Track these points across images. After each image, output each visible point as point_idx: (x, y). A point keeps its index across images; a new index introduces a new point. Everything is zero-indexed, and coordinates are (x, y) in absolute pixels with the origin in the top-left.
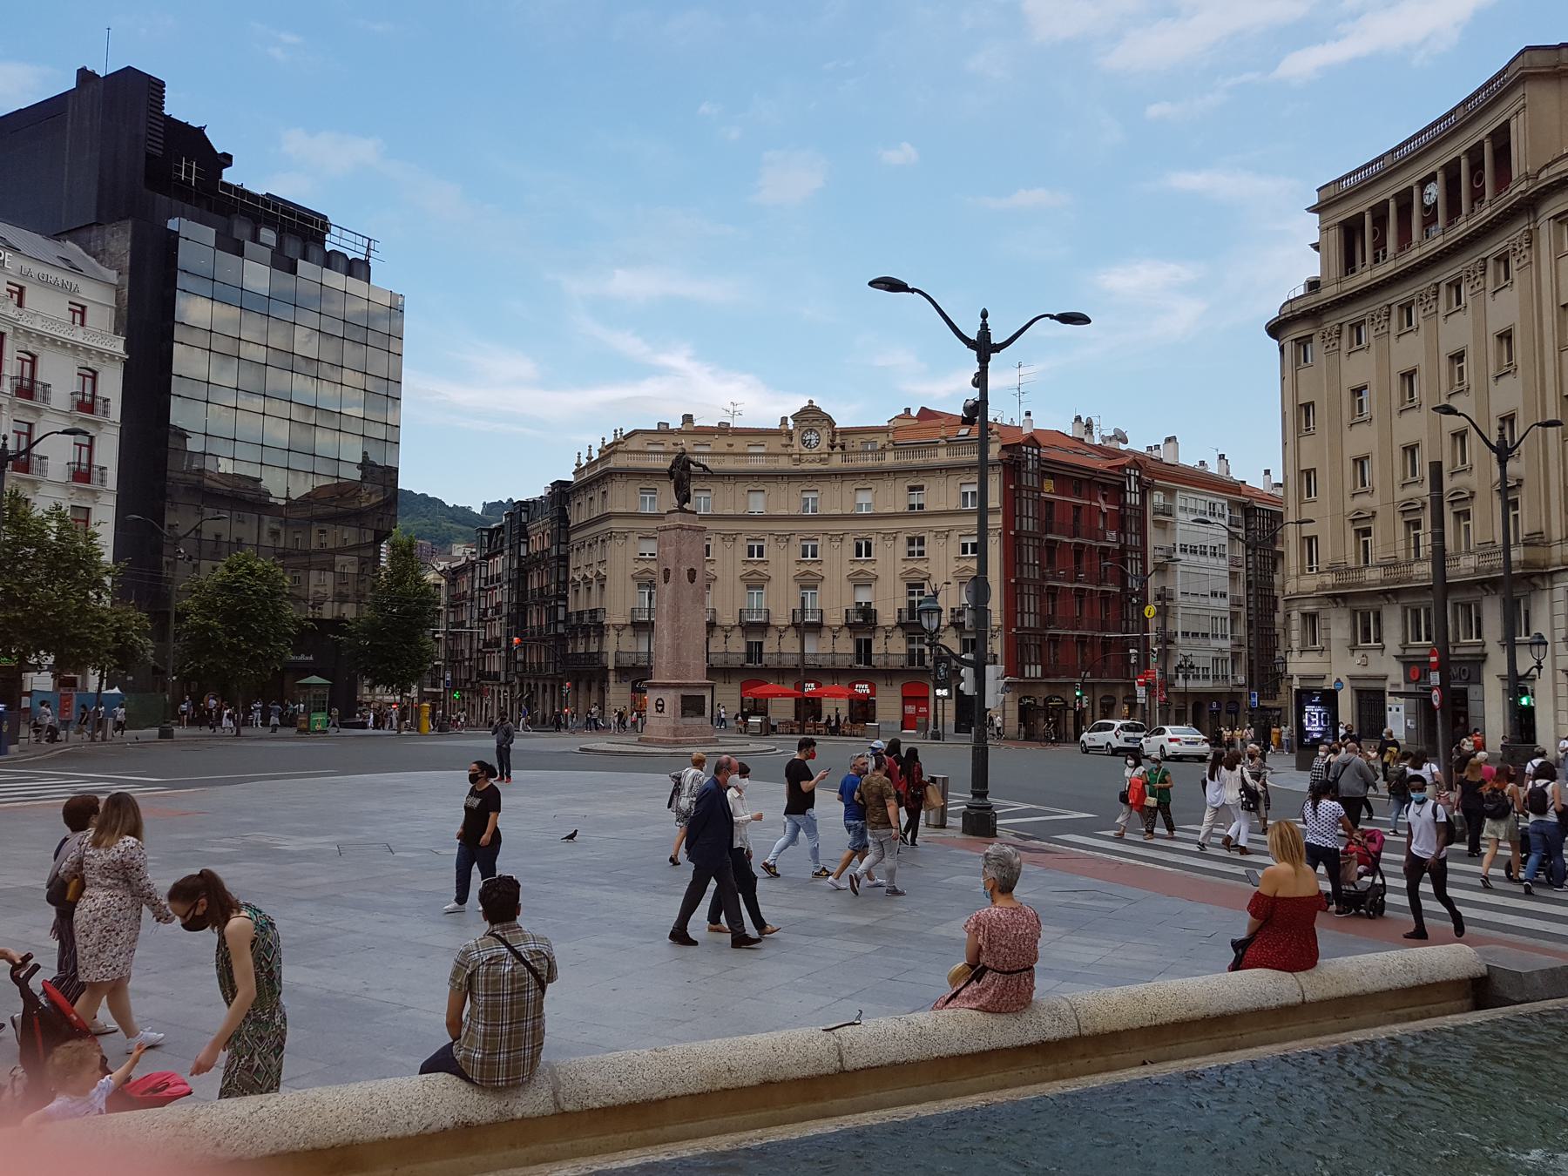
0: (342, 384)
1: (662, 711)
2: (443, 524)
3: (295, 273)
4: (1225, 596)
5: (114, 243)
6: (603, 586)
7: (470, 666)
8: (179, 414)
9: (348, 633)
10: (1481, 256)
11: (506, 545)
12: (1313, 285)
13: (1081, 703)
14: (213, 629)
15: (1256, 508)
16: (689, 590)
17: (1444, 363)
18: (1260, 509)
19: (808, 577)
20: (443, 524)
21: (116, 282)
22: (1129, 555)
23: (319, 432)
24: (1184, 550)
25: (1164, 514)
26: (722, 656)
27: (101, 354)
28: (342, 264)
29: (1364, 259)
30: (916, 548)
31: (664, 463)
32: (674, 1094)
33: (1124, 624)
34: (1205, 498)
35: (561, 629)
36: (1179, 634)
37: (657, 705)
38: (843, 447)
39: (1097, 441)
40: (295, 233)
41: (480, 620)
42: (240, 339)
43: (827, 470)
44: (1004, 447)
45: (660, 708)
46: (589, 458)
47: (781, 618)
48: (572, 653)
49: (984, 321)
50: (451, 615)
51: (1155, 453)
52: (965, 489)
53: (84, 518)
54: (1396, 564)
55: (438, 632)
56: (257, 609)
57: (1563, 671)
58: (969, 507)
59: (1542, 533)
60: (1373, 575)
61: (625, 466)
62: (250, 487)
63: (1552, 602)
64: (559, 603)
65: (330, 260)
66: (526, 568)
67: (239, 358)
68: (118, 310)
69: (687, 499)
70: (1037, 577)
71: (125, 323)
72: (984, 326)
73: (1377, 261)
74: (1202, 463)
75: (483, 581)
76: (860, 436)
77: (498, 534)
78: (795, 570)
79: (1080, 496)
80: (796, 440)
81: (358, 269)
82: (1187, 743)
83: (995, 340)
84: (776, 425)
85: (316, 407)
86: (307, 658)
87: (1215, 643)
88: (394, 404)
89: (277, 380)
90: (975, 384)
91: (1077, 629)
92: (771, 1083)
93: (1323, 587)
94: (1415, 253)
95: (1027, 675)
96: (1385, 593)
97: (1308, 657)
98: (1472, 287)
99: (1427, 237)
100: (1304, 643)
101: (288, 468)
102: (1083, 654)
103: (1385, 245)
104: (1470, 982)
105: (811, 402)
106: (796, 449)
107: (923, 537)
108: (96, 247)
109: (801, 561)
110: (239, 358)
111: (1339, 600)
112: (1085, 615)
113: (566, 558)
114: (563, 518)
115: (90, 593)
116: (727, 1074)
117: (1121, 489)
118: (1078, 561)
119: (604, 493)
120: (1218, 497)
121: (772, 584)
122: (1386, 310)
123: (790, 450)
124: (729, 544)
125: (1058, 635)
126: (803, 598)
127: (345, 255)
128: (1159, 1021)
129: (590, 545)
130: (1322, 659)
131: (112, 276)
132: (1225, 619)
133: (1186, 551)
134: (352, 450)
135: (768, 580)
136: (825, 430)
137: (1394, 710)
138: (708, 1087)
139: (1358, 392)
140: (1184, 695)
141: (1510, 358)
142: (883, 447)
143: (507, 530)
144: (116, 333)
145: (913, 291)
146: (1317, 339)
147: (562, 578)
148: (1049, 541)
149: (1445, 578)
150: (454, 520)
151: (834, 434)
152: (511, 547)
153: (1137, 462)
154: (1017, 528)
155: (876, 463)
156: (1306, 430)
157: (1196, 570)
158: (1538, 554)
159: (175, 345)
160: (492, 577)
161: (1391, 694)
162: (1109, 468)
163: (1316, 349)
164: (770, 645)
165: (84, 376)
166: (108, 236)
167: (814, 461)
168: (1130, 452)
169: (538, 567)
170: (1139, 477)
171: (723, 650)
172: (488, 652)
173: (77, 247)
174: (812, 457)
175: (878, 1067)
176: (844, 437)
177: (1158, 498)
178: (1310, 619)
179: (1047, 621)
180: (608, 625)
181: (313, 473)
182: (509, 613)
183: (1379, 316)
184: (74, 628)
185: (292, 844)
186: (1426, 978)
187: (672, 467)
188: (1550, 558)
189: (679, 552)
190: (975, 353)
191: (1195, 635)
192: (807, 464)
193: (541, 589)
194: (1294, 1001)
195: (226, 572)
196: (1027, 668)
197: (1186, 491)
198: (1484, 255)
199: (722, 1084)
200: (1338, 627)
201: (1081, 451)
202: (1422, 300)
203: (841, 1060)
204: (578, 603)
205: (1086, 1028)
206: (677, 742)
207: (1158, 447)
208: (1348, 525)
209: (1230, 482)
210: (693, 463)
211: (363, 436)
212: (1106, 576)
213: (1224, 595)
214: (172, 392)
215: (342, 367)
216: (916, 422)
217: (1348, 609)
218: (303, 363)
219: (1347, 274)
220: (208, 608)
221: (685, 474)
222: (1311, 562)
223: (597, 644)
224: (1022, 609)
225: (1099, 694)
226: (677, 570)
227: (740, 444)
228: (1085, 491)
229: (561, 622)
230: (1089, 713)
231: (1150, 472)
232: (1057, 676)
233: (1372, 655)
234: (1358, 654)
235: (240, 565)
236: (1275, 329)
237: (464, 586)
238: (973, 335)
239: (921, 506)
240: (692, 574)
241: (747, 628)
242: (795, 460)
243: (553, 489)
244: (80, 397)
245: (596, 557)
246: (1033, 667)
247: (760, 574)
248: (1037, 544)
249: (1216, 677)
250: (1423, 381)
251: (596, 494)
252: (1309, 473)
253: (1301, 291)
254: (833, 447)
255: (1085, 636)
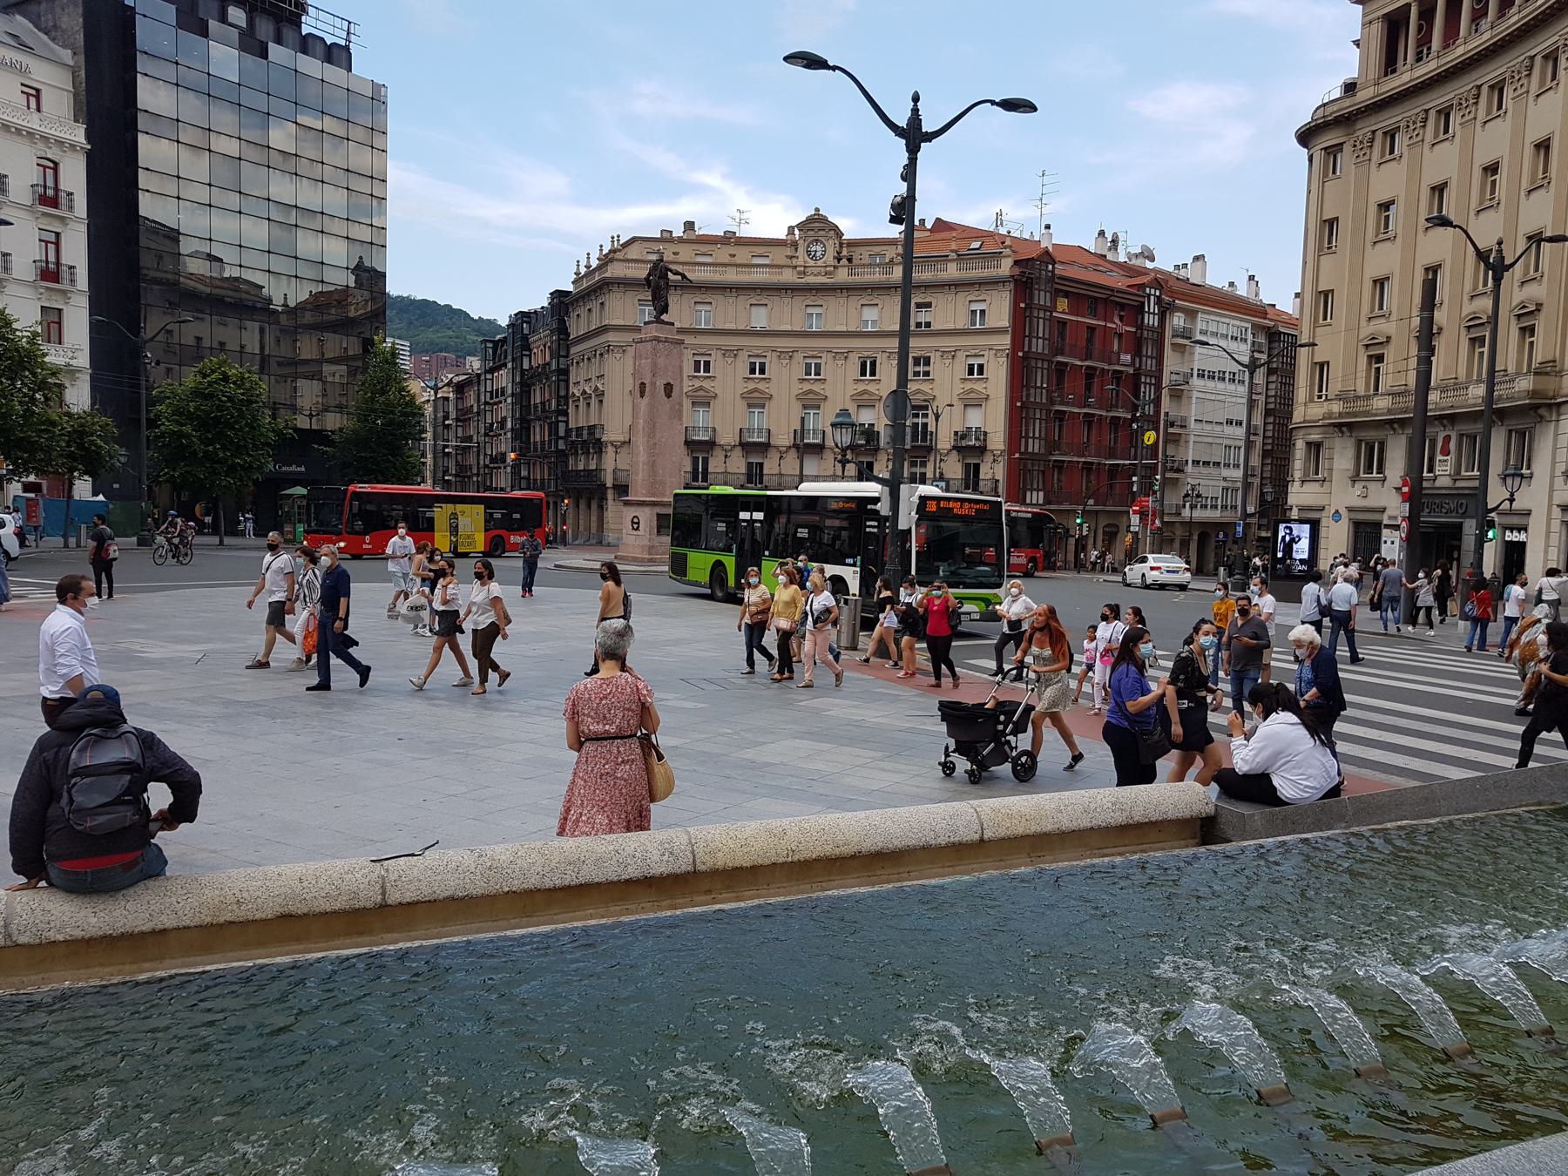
0: (323, 182)
1: (638, 529)
2: (468, 337)
3: (266, 57)
4: (1241, 424)
5: (65, 19)
6: (601, 401)
7: (478, 481)
8: (148, 207)
9: (331, 443)
10: (1528, 54)
11: (510, 357)
12: (1350, 88)
13: (1081, 530)
14: (187, 436)
15: (1281, 333)
16: (665, 404)
17: (1477, 173)
18: (1285, 334)
19: (811, 396)
20: (468, 337)
21: (71, 63)
22: (1143, 380)
23: (300, 231)
24: (1201, 375)
25: (1183, 337)
26: (776, 478)
27: (60, 143)
28: (319, 49)
29: (1405, 59)
30: (921, 369)
31: (642, 272)
32: (162, 927)
33: (1133, 450)
34: (1227, 320)
35: (561, 445)
36: (1190, 462)
37: (633, 522)
38: (850, 260)
39: (1122, 258)
40: (269, 13)
41: (486, 435)
42: (209, 130)
43: (833, 284)
44: (1016, 263)
45: (635, 526)
46: (588, 267)
47: (783, 439)
48: (584, 470)
49: (916, 105)
50: (460, 429)
51: (1183, 273)
52: (974, 307)
53: (57, 320)
54: (1406, 391)
55: (447, 446)
56: (232, 417)
57: (1558, 506)
58: (978, 326)
59: (1555, 361)
60: (1381, 404)
61: (622, 275)
62: (252, 293)
63: (1556, 435)
64: (560, 419)
65: (307, 44)
66: (529, 382)
67: (210, 150)
68: (76, 95)
69: (665, 309)
70: (1044, 401)
71: (85, 108)
72: (915, 111)
73: (1419, 59)
74: (1232, 284)
75: (488, 394)
76: (871, 248)
77: (502, 346)
78: (797, 388)
79: (1095, 316)
80: (801, 250)
81: (337, 55)
82: (1168, 571)
83: (927, 127)
84: (781, 234)
85: (296, 206)
86: (299, 469)
87: (1225, 472)
88: (379, 203)
89: (252, 178)
90: (904, 178)
91: (1083, 456)
92: (291, 916)
93: (1330, 415)
94: (1460, 51)
95: (1028, 501)
96: (1391, 422)
97: (1309, 487)
98: (1515, 90)
99: (1476, 31)
100: (1306, 473)
101: (269, 271)
102: (1088, 481)
103: (1431, 41)
104: (1199, 822)
105: (817, 210)
106: (800, 261)
107: (929, 357)
108: (46, 21)
109: (748, 379)
110: (210, 150)
111: (1344, 429)
112: (1093, 440)
113: (566, 372)
114: (563, 330)
115: (37, 396)
116: (235, 907)
117: (1140, 310)
118: (1089, 387)
119: (602, 304)
120: (1242, 320)
121: (774, 403)
122: (1422, 115)
123: (794, 262)
124: (730, 360)
125: (1063, 462)
126: (803, 419)
127: (322, 39)
128: (796, 858)
129: (589, 359)
130: (1322, 490)
131: (66, 55)
132: (1239, 448)
133: (1203, 376)
134: (337, 253)
135: (715, 397)
136: (831, 242)
137: (1389, 543)
138: (208, 919)
139: (1385, 206)
140: (1190, 524)
141: (1545, 171)
142: (891, 261)
143: (510, 341)
144: (76, 121)
145: (834, 68)
146: (1347, 148)
147: (562, 393)
148: (1059, 363)
149: (1426, 410)
150: (479, 332)
151: (841, 245)
152: (513, 360)
153: (1160, 281)
154: (1026, 349)
155: (884, 277)
156: (1329, 248)
157: (1213, 397)
158: (1549, 384)
159: (140, 136)
160: (497, 390)
161: (1387, 526)
162: (1128, 286)
163: (1346, 159)
164: (771, 466)
165: (45, 167)
166: (58, 10)
167: (819, 274)
168: (1154, 270)
169: (541, 381)
170: (1159, 297)
171: (777, 472)
172: (495, 468)
173: (26, 22)
174: (818, 269)
175: (429, 901)
176: (853, 249)
177: (1178, 320)
178: (1315, 448)
179: (1052, 446)
180: (606, 442)
181: (296, 277)
182: (512, 428)
183: (1414, 123)
184: (21, 431)
185: (156, 651)
186: (1138, 817)
187: (649, 275)
188: (1560, 388)
189: (655, 365)
190: (904, 141)
191: (1206, 463)
192: (811, 277)
193: (543, 403)
194: (968, 838)
195: (199, 378)
196: (1028, 494)
197: (1209, 313)
198: (1532, 53)
199: (229, 917)
200: (1342, 457)
201: (1101, 268)
202: (1461, 104)
203: (384, 894)
204: (578, 418)
205: (704, 863)
206: (651, 560)
207: (1185, 266)
208: (1362, 350)
209: (1256, 305)
210: (671, 271)
211: (347, 238)
212: (1117, 401)
213: (1239, 423)
214: (140, 186)
215: (323, 163)
216: (928, 233)
217: (1353, 439)
218: (280, 158)
219: (1386, 75)
220: (180, 413)
221: (662, 283)
222: (1320, 390)
223: (595, 461)
224: (1027, 433)
225: (1103, 522)
226: (653, 384)
227: (743, 255)
228: (1100, 310)
229: (561, 438)
230: (1091, 541)
231: (1172, 293)
232: (1059, 503)
233: (1372, 486)
234: (1359, 485)
235: (213, 372)
236: (1306, 137)
237: (471, 400)
238: (902, 122)
239: (928, 325)
240: (669, 389)
241: (747, 447)
242: (799, 273)
243: (552, 299)
244: (41, 190)
245: (593, 374)
246: (1035, 493)
247: (761, 392)
248: (1046, 366)
249: (1224, 507)
250: (1453, 195)
251: (594, 305)
252: (1327, 294)
253: (1337, 94)
254: (839, 260)
255: (1092, 463)
